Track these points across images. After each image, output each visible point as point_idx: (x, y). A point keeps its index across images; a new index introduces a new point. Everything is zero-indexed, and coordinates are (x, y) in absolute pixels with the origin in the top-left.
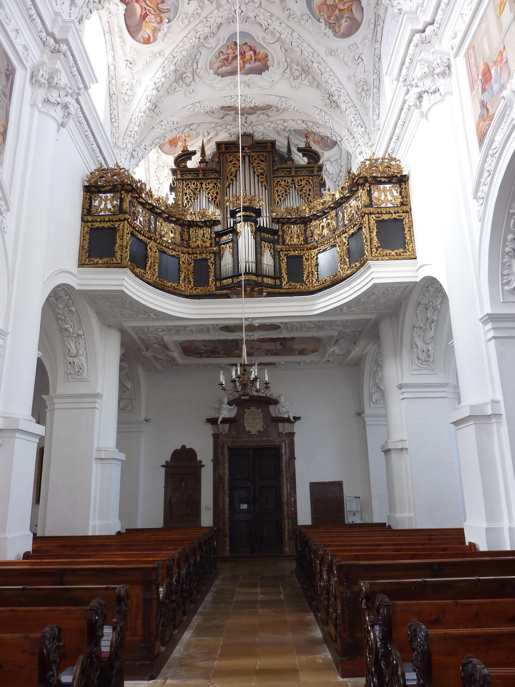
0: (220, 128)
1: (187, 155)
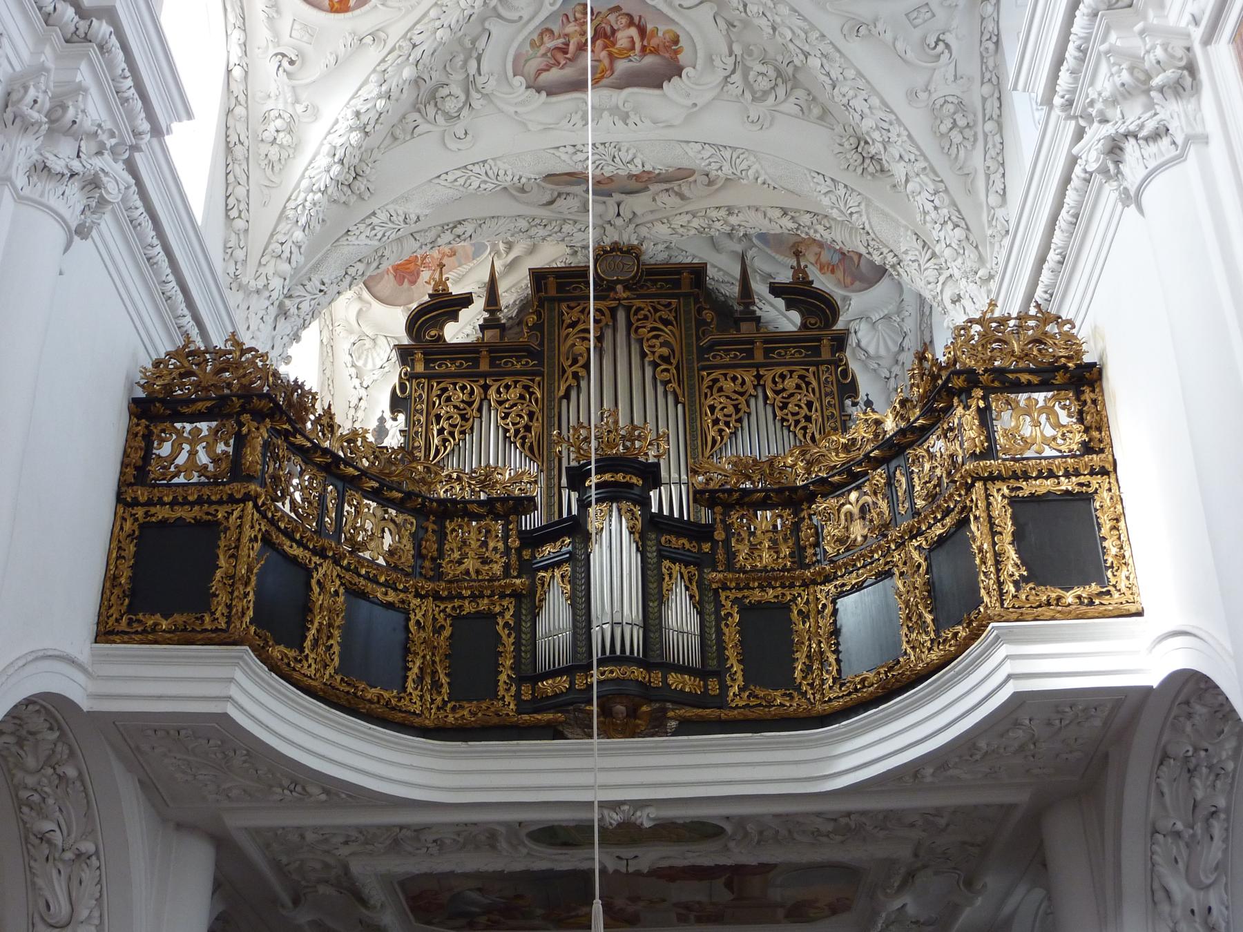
0: (542, 232)
1: (446, 305)
